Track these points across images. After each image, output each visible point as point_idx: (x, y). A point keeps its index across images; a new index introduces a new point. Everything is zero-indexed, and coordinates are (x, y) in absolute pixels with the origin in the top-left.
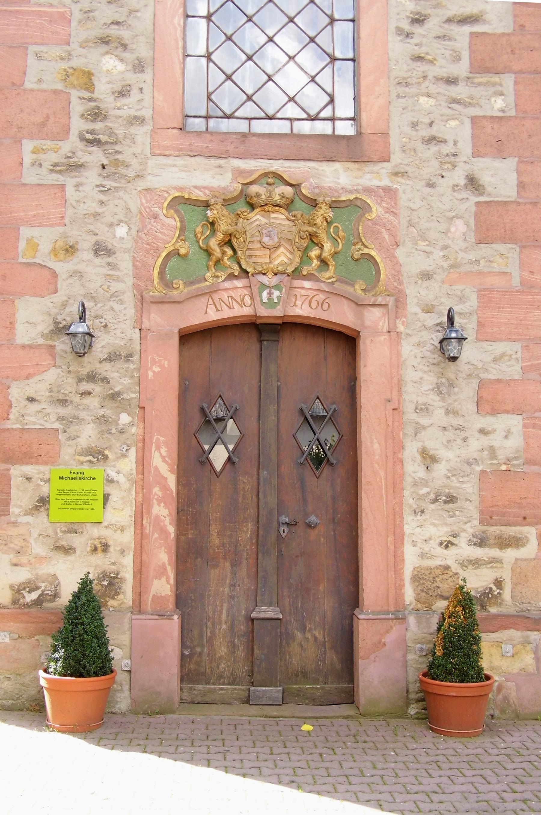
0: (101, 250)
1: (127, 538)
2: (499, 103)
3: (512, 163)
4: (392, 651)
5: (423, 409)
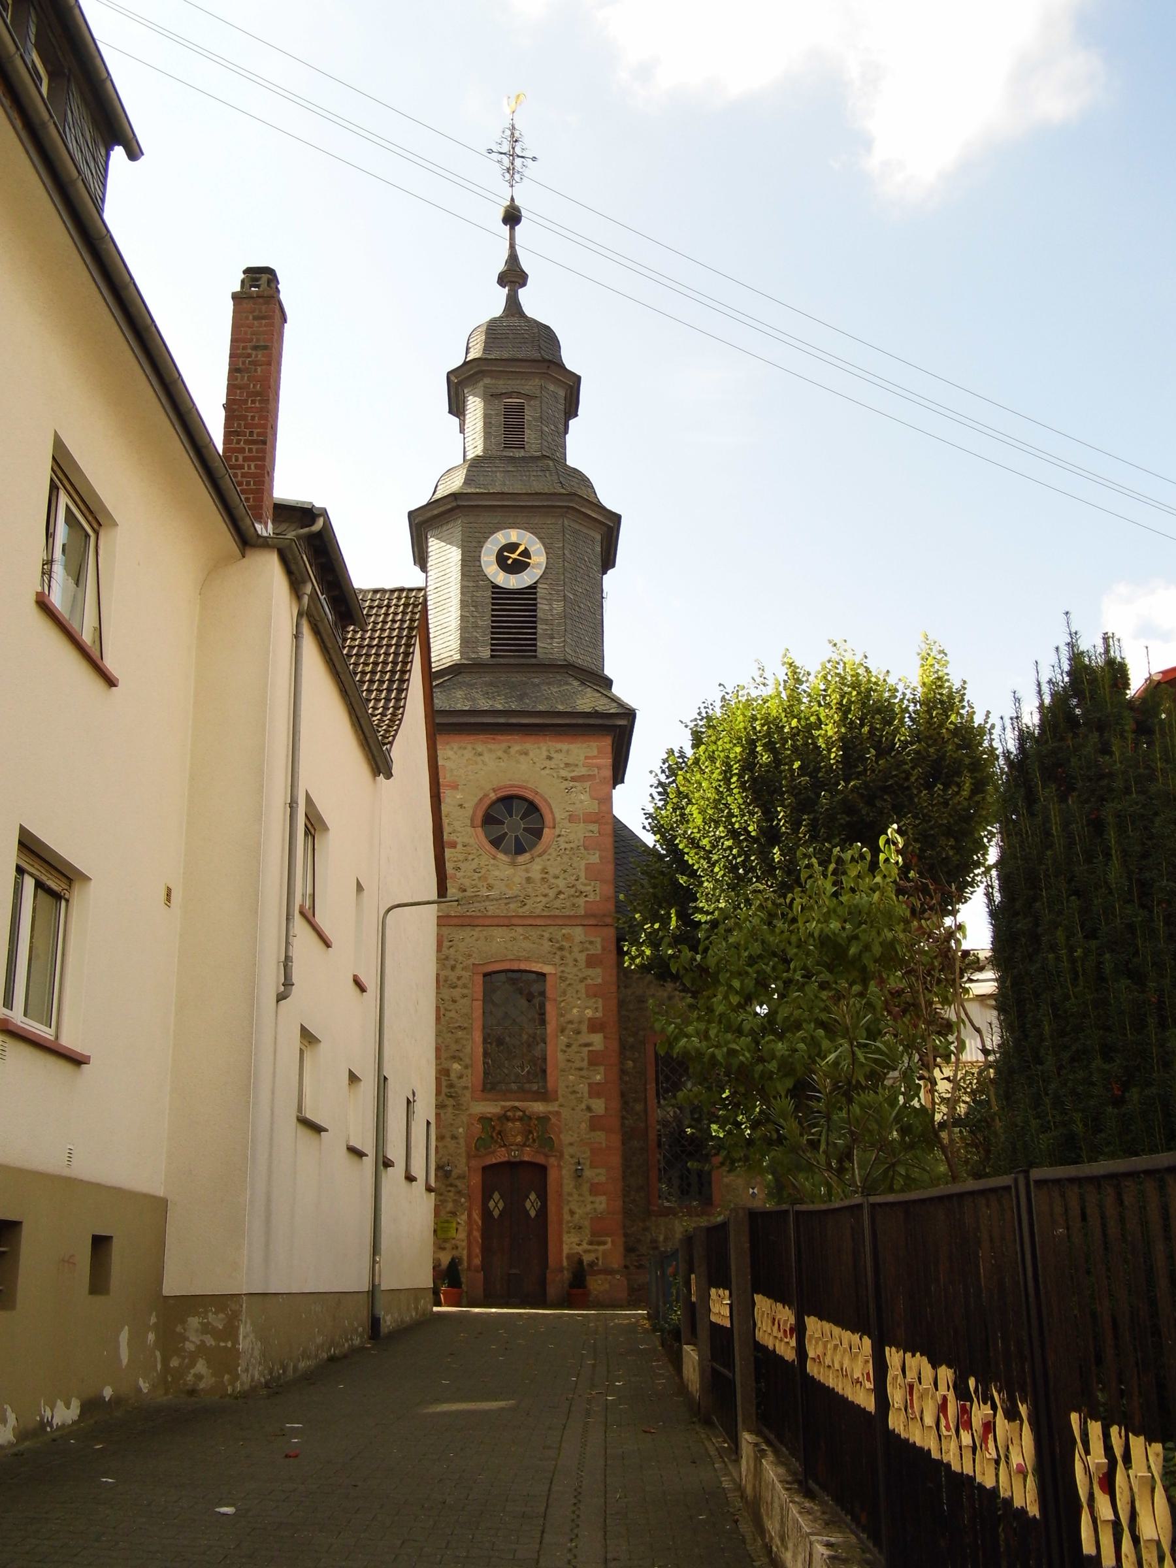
0: (454, 1137)
1: (464, 1244)
2: (598, 1077)
3: (603, 1099)
4: (557, 1282)
5: (570, 1194)
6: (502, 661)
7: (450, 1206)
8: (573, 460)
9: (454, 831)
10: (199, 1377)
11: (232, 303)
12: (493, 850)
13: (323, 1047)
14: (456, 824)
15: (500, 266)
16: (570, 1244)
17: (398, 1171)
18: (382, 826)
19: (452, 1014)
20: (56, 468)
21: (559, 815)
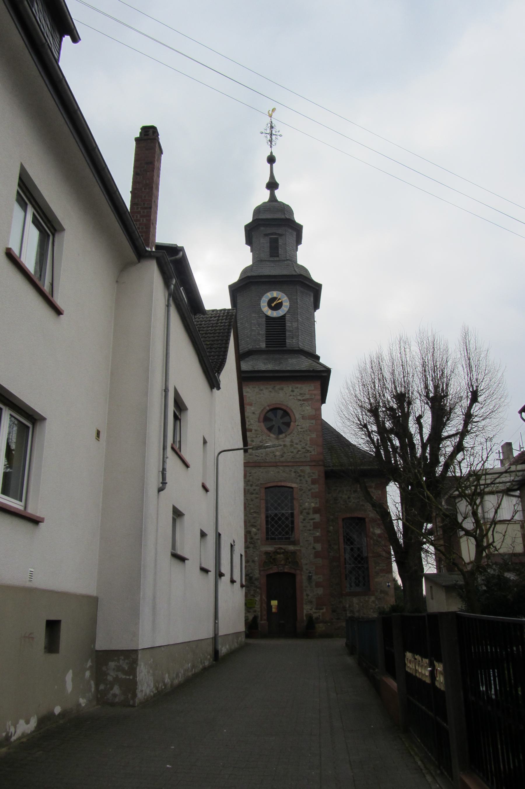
0: (253, 561)
1: (259, 610)
2: (318, 534)
6: (271, 349)
7: (252, 592)
8: (300, 261)
9: (251, 424)
10: (115, 695)
11: (135, 143)
12: (268, 433)
13: (186, 518)
14: (252, 422)
15: (267, 180)
16: (307, 609)
17: (226, 579)
18: (217, 414)
19: (251, 506)
20: (22, 185)
21: (298, 416)
